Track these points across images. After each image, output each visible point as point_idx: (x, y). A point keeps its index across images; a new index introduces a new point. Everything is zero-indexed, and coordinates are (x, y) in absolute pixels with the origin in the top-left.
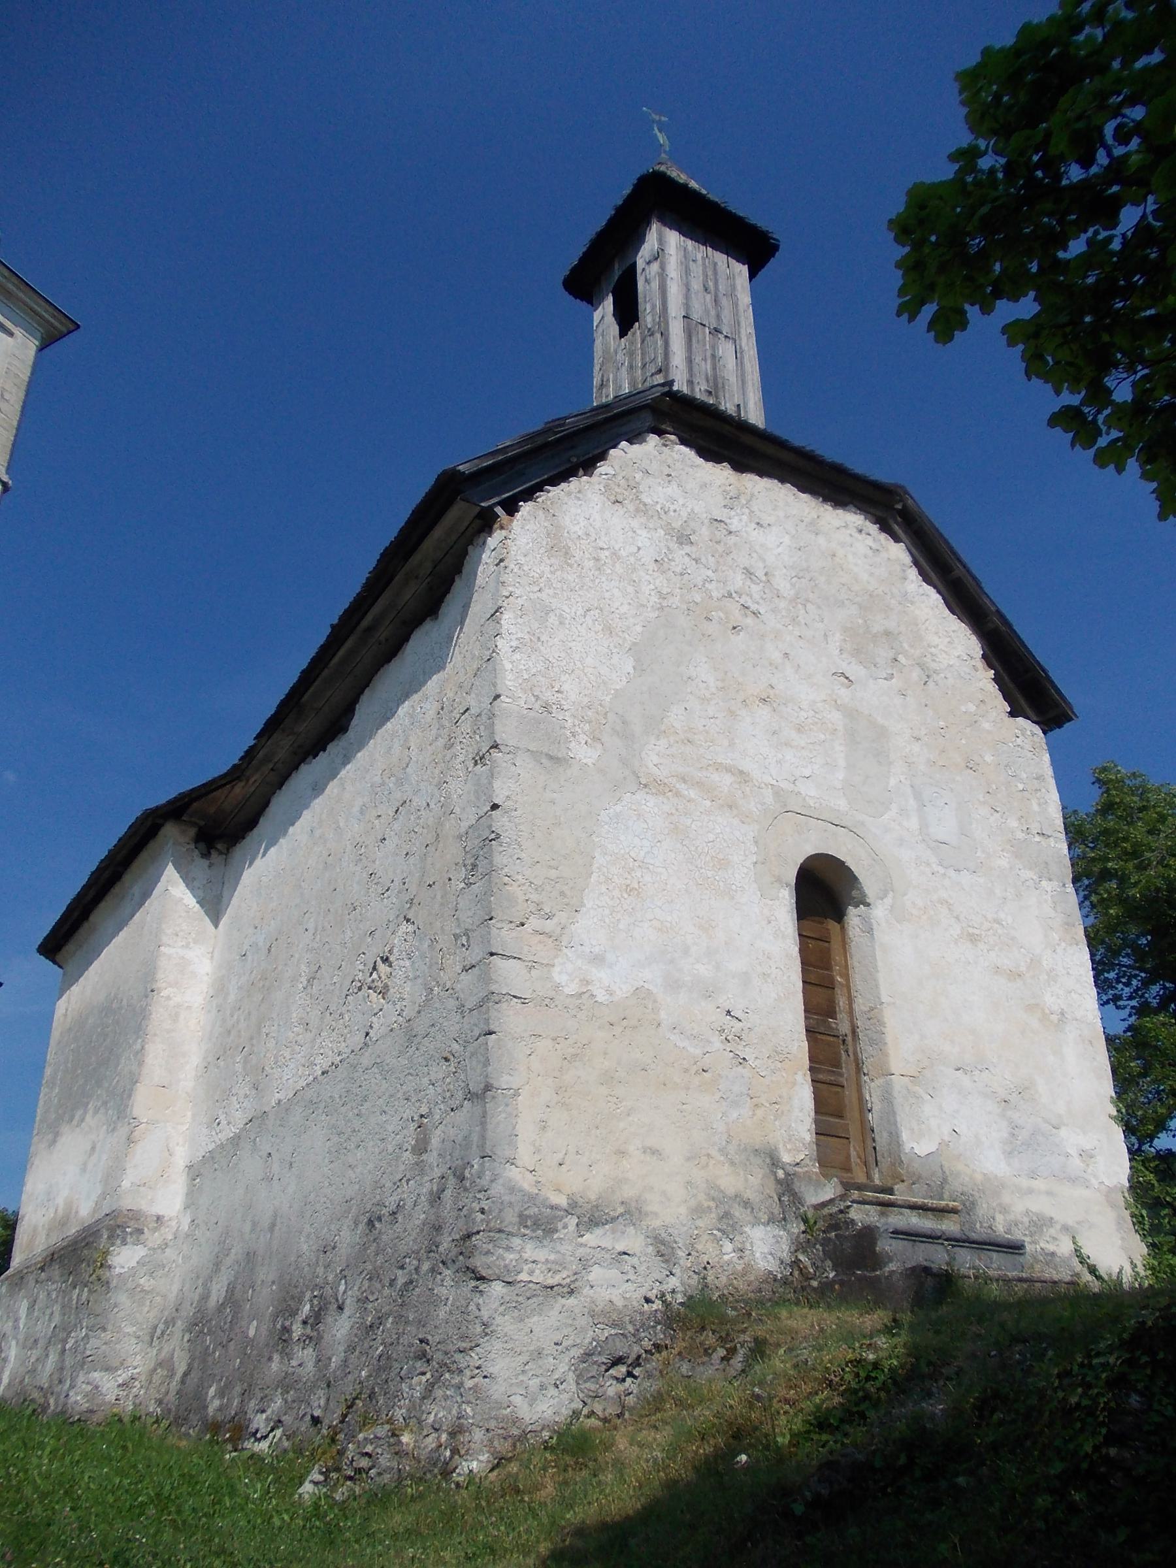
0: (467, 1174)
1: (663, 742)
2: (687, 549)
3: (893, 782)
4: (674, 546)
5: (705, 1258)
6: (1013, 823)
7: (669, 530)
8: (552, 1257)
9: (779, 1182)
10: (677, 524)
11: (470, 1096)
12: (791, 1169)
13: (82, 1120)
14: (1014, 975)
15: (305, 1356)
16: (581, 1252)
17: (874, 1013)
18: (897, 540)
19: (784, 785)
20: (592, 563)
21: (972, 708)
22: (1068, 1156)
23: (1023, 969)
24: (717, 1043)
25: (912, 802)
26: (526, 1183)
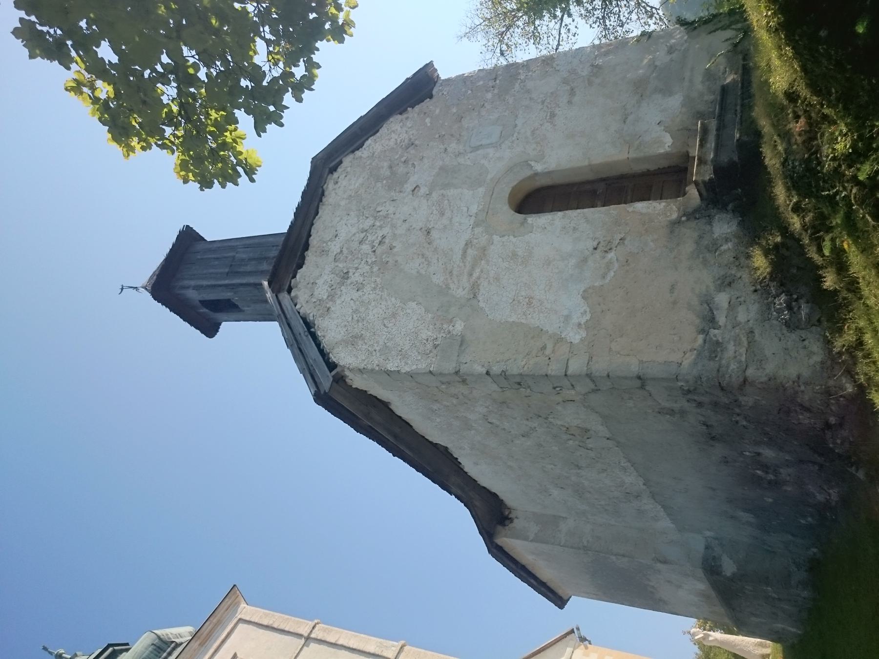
0: (686, 388)
1: (452, 286)
2: (351, 274)
3: (469, 163)
4: (349, 281)
5: (732, 259)
6: (489, 96)
7: (342, 284)
8: (732, 343)
9: (688, 220)
10: (338, 280)
11: (643, 387)
12: (682, 213)
13: (653, 587)
14: (572, 92)
15: (785, 473)
16: (729, 327)
17: (591, 167)
18: (341, 162)
19: (472, 222)
20: (360, 324)
21: (428, 120)
22: (672, 60)
23: (569, 88)
24: (611, 255)
25: (478, 152)
26: (690, 358)
